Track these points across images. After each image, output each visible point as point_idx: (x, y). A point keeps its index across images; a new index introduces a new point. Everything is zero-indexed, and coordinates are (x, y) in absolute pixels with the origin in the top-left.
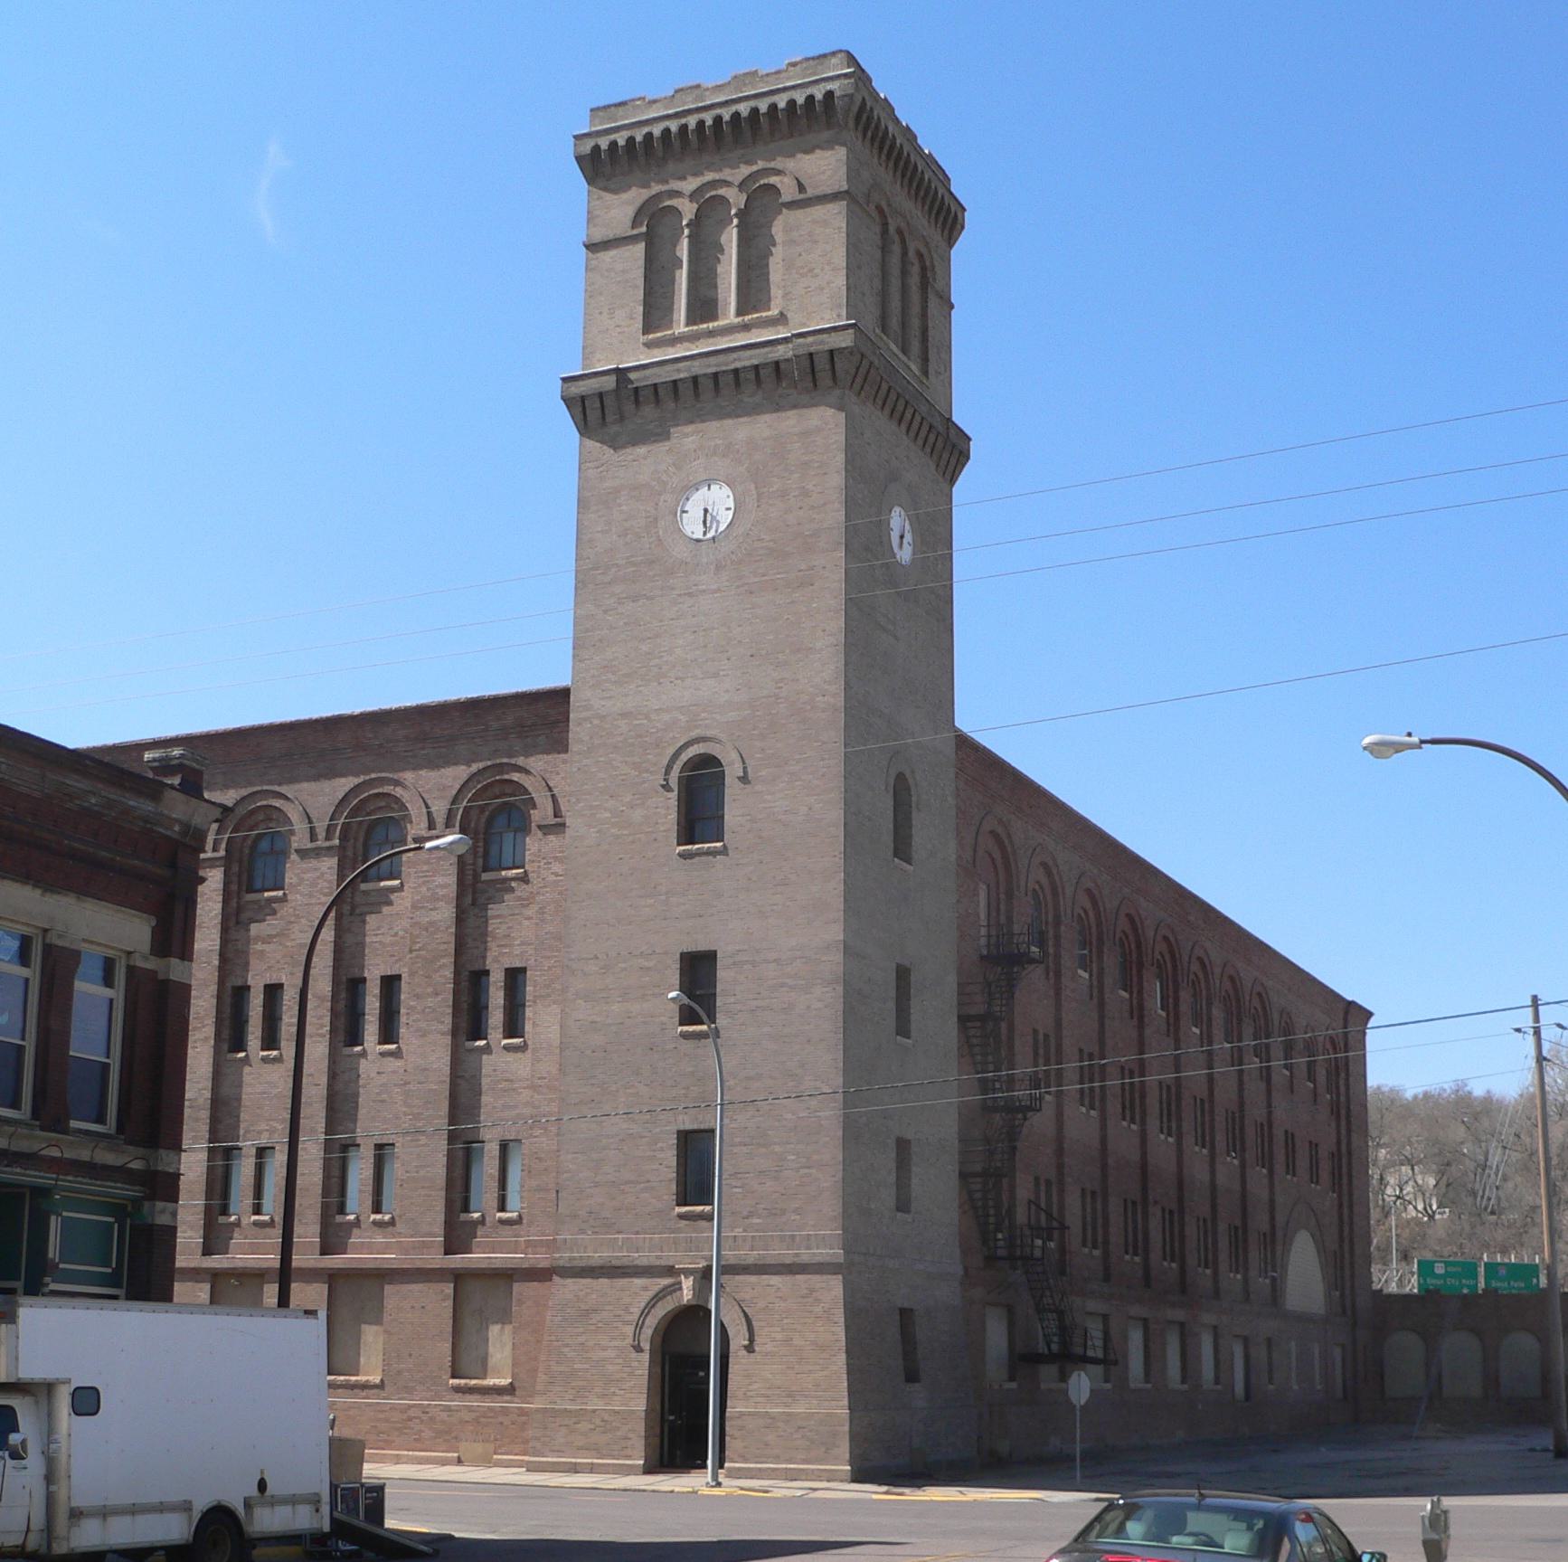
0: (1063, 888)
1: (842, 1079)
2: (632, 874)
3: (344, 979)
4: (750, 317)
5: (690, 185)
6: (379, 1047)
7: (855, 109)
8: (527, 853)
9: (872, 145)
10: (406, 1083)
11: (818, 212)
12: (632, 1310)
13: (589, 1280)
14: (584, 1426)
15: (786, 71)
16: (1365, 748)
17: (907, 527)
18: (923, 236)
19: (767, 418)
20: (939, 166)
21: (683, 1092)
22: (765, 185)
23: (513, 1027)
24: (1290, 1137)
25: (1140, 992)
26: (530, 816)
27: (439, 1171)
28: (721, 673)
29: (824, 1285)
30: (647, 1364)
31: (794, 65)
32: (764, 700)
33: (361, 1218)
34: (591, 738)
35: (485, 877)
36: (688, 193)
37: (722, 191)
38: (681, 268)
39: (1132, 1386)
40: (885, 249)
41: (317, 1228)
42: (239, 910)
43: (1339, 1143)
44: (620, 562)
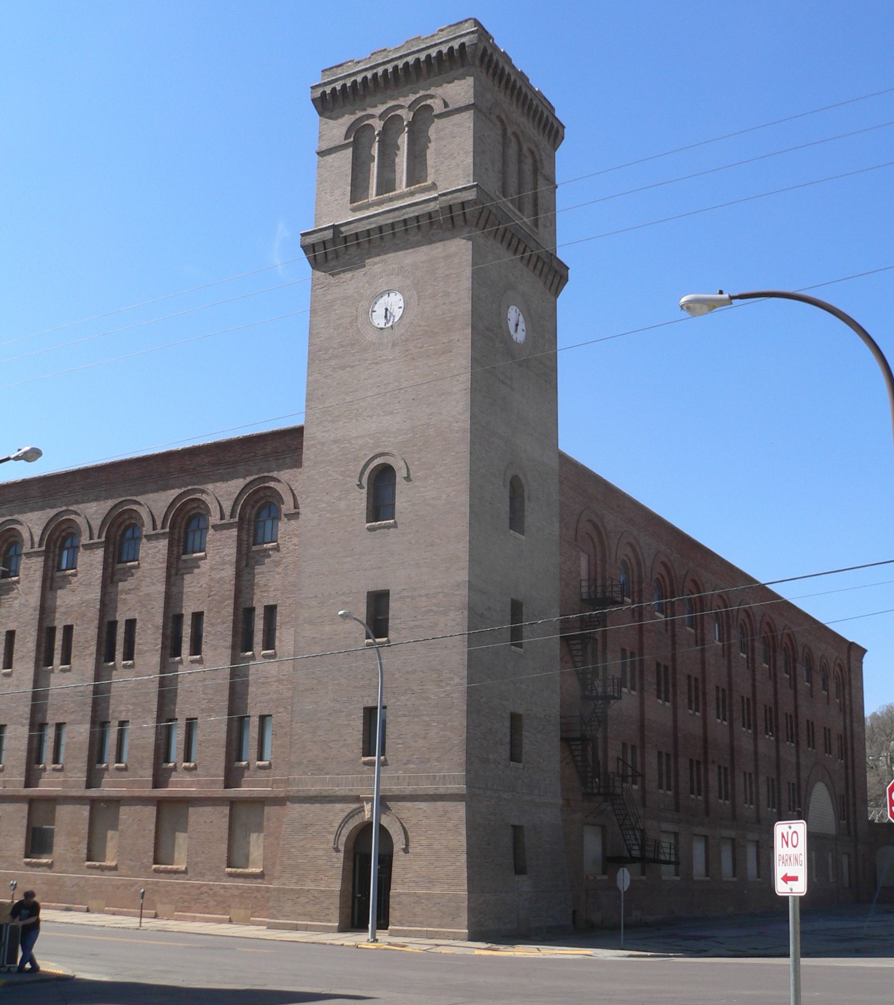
0: (644, 560)
1: (466, 672)
2: (339, 542)
3: (171, 615)
4: (414, 187)
5: (380, 109)
6: (190, 657)
7: (479, 53)
8: (279, 532)
9: (544, 133)
10: (204, 680)
11: (456, 118)
12: (334, 825)
13: (308, 805)
14: (303, 900)
15: (437, 34)
16: (682, 307)
17: (521, 319)
18: (534, 141)
19: (424, 249)
20: (546, 100)
21: (368, 682)
22: (424, 105)
23: (269, 643)
24: (810, 725)
25: (702, 630)
26: (281, 509)
27: (223, 735)
28: (395, 411)
29: (453, 808)
30: (342, 860)
31: (442, 30)
32: (421, 427)
33: (177, 765)
34: (316, 457)
35: (254, 548)
36: (378, 115)
37: (399, 112)
38: (374, 161)
39: (695, 878)
40: (505, 145)
41: (150, 772)
42: (113, 574)
43: (845, 728)
44: (335, 346)
